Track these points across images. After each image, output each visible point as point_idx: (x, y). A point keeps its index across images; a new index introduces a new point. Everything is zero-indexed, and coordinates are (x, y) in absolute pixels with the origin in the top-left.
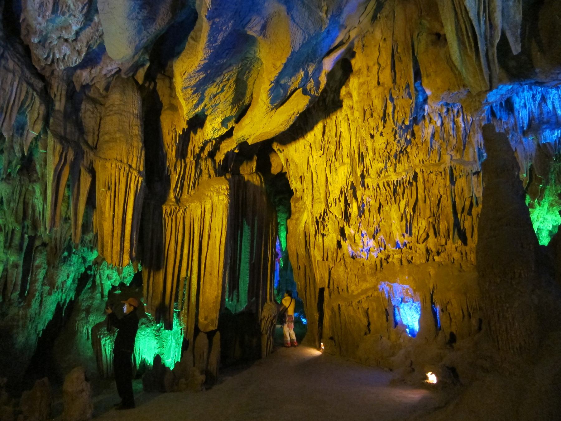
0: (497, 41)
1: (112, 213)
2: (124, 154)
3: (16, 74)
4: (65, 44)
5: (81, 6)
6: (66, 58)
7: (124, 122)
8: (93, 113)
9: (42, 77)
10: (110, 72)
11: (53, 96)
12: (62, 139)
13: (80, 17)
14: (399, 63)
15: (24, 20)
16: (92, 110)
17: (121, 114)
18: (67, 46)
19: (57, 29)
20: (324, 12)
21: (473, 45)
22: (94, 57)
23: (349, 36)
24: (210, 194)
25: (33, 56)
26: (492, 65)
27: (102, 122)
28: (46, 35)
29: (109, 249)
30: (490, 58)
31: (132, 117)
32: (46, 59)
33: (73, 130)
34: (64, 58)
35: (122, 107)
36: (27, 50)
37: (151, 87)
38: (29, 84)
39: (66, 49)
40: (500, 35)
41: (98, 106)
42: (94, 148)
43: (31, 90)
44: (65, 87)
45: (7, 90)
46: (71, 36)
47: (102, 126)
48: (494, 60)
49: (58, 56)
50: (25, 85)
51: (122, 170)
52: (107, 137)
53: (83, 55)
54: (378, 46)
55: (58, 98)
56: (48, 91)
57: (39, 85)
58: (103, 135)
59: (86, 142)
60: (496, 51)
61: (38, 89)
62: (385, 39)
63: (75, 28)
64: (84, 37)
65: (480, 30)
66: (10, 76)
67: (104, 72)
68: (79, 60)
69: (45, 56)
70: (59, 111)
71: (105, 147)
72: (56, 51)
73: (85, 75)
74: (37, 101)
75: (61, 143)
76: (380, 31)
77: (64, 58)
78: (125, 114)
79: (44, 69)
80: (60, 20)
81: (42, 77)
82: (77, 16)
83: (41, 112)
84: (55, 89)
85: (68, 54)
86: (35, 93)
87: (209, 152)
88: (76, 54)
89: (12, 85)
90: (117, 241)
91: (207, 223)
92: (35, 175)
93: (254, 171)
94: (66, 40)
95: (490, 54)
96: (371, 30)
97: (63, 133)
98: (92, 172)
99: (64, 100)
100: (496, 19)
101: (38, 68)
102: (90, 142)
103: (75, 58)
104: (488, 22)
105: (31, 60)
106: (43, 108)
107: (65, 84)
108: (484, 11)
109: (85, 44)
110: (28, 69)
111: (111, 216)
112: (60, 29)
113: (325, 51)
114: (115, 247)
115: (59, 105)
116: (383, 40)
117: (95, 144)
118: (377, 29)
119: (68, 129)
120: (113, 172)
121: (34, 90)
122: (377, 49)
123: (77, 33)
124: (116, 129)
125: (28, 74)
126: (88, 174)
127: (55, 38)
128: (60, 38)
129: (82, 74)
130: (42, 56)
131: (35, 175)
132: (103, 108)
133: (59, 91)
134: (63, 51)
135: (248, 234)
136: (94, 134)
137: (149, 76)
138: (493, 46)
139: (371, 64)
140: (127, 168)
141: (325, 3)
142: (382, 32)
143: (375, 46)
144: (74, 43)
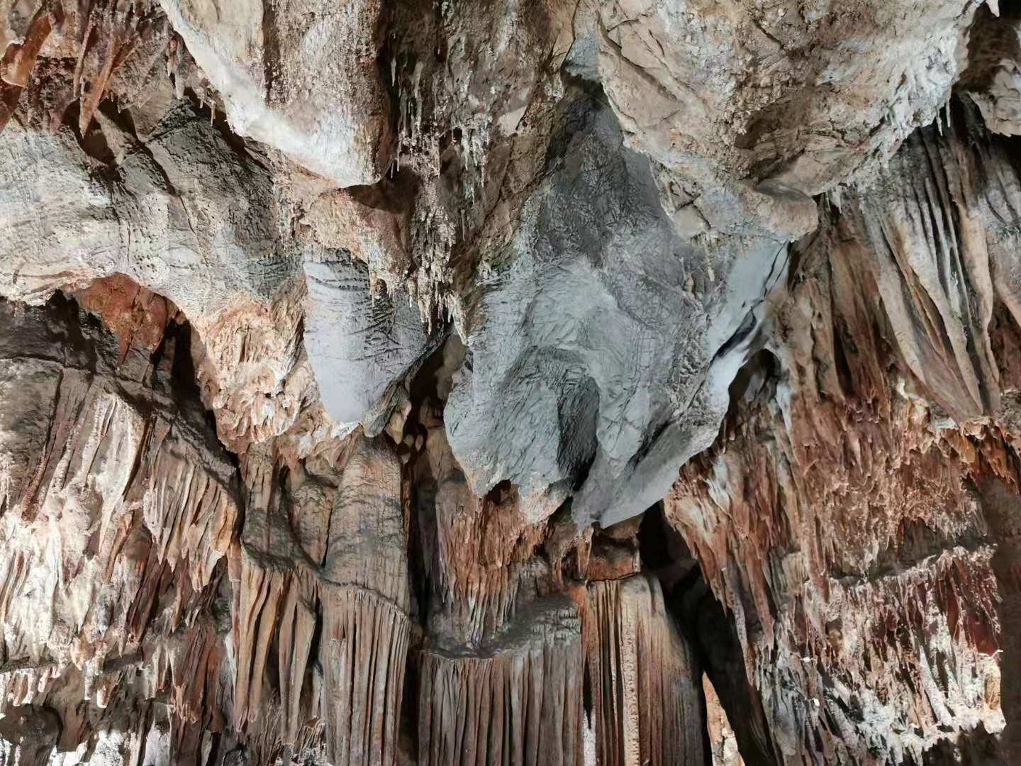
0: (987, 320)
1: (349, 684)
2: (370, 574)
3: (190, 461)
4: (267, 401)
5: (284, 344)
6: (268, 423)
7: (369, 515)
8: (318, 504)
9: (233, 459)
10: (346, 431)
11: (250, 487)
12: (264, 558)
13: (288, 361)
14: (853, 355)
15: (203, 374)
16: (316, 499)
17: (363, 502)
18: (268, 405)
19: (253, 382)
20: (690, 289)
21: (938, 334)
22: (308, 414)
23: (754, 318)
24: (539, 628)
25: (219, 428)
26: (984, 365)
27: (333, 518)
28: (236, 393)
29: (344, 753)
30: (980, 352)
31: (382, 504)
32: (237, 429)
33: (283, 538)
34: (265, 424)
35: (364, 489)
36: (210, 416)
37: (418, 447)
38: (211, 473)
39: (267, 409)
40: (990, 308)
41: (327, 490)
42: (322, 566)
43: (213, 482)
44: (270, 469)
45: (176, 489)
46: (274, 390)
47: (333, 525)
48: (986, 355)
49: (255, 422)
50: (204, 476)
51: (366, 602)
52: (339, 546)
53: (294, 415)
54: (809, 329)
55: (258, 488)
56: (243, 478)
57: (227, 471)
58: (335, 541)
59: (307, 557)
60: (988, 339)
61: (224, 478)
62: (820, 316)
63: (279, 376)
64: (294, 388)
65: (950, 304)
66: (181, 466)
67: (334, 434)
68: (291, 423)
69: (236, 425)
70: (260, 510)
71: (337, 563)
72: (253, 415)
73: (304, 445)
74: (224, 497)
75: (262, 567)
76: (808, 303)
77: (265, 424)
78: (370, 501)
79: (235, 444)
80: (251, 367)
81: (233, 459)
82: (280, 358)
83: (230, 518)
84: (254, 474)
85: (270, 417)
86: (220, 486)
87: (535, 547)
88: (284, 416)
89: (183, 480)
90: (357, 735)
91: (538, 687)
92: (227, 620)
93: (637, 570)
94: (268, 396)
95: (978, 345)
96: (790, 301)
97: (265, 548)
98: (316, 609)
99: (267, 490)
100: (978, 281)
101: (227, 445)
102: (314, 556)
103: (281, 422)
104: (964, 287)
105: (215, 432)
106: (233, 509)
107: (269, 464)
108: (954, 268)
109: (297, 397)
110: (208, 448)
111: (348, 689)
112: (256, 380)
113: (715, 348)
114: (354, 749)
115: (260, 501)
116: (815, 317)
117: (322, 557)
118: (803, 299)
119: (274, 539)
120: (351, 606)
121: (219, 481)
122: (808, 333)
123: (284, 383)
124: (356, 529)
125: (208, 456)
126: (309, 615)
127: (250, 395)
128: (257, 393)
129: (298, 441)
130: (230, 426)
131: (227, 620)
132: (334, 492)
133: (259, 473)
134: (263, 413)
135: (631, 702)
136: (319, 539)
137: (413, 426)
138: (980, 331)
139: (803, 362)
140: (374, 598)
141: (690, 275)
142: (812, 305)
143: (805, 328)
144: (280, 397)
